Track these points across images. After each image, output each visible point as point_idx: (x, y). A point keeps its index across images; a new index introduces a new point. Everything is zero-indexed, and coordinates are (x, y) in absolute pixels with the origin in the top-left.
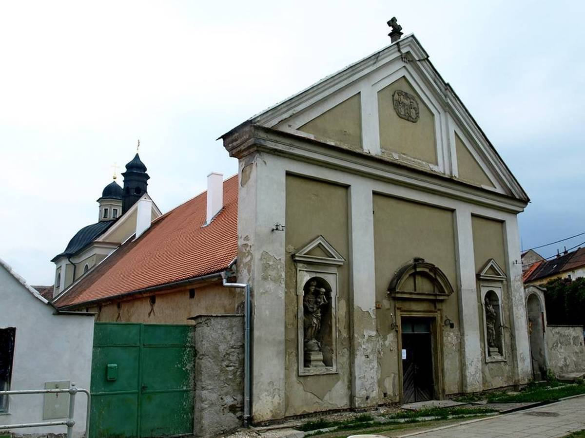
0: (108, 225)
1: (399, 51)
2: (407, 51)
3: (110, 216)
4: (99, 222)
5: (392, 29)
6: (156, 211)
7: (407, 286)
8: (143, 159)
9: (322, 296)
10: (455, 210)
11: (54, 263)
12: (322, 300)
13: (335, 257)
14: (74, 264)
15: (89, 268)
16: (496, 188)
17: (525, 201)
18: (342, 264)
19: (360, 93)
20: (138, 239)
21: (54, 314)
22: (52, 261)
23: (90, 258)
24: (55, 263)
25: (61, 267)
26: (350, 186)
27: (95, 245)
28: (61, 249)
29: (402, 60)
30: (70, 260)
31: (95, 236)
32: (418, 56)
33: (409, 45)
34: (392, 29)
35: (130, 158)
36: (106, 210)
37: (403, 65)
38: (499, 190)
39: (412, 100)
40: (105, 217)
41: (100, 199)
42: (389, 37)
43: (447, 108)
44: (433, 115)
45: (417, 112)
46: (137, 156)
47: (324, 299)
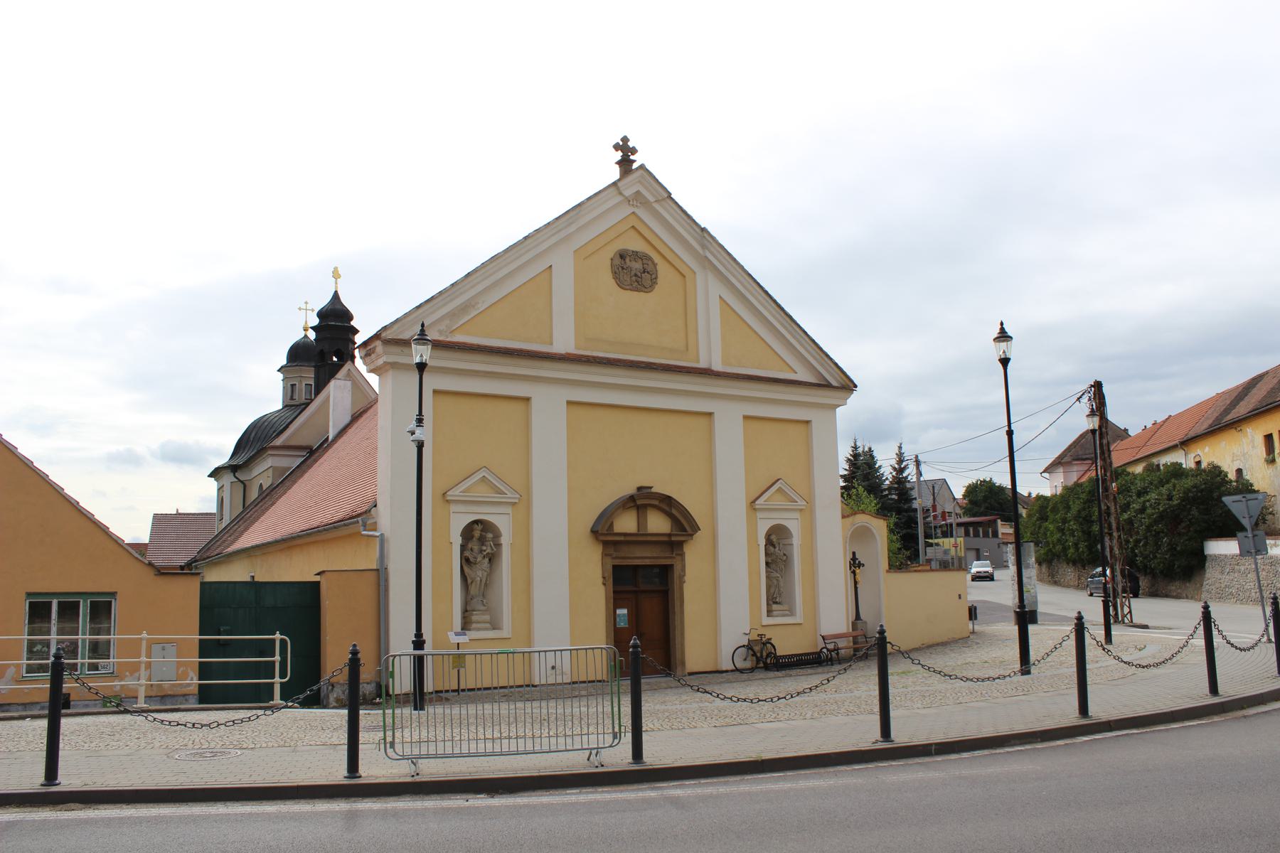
0: (299, 411)
1: (621, 193)
2: (634, 191)
3: (301, 396)
4: (283, 408)
5: (621, 154)
6: (367, 389)
7: (626, 523)
8: (347, 301)
9: (488, 543)
10: (713, 413)
11: (213, 479)
12: (489, 548)
13: (506, 492)
14: (242, 482)
15: (264, 489)
16: (796, 373)
17: (848, 386)
18: (517, 501)
19: (551, 266)
20: (331, 442)
21: (156, 575)
22: (209, 476)
23: (262, 474)
24: (215, 480)
25: (223, 486)
26: (531, 398)
27: (270, 452)
28: (223, 460)
29: (629, 204)
30: (236, 474)
31: (275, 434)
32: (654, 196)
33: (640, 182)
34: (621, 154)
35: (323, 301)
36: (293, 386)
37: (632, 211)
38: (803, 375)
39: (645, 261)
40: (292, 398)
41: (282, 367)
42: (617, 166)
43: (706, 263)
44: (695, 273)
45: (653, 276)
46: (336, 296)
47: (491, 546)
